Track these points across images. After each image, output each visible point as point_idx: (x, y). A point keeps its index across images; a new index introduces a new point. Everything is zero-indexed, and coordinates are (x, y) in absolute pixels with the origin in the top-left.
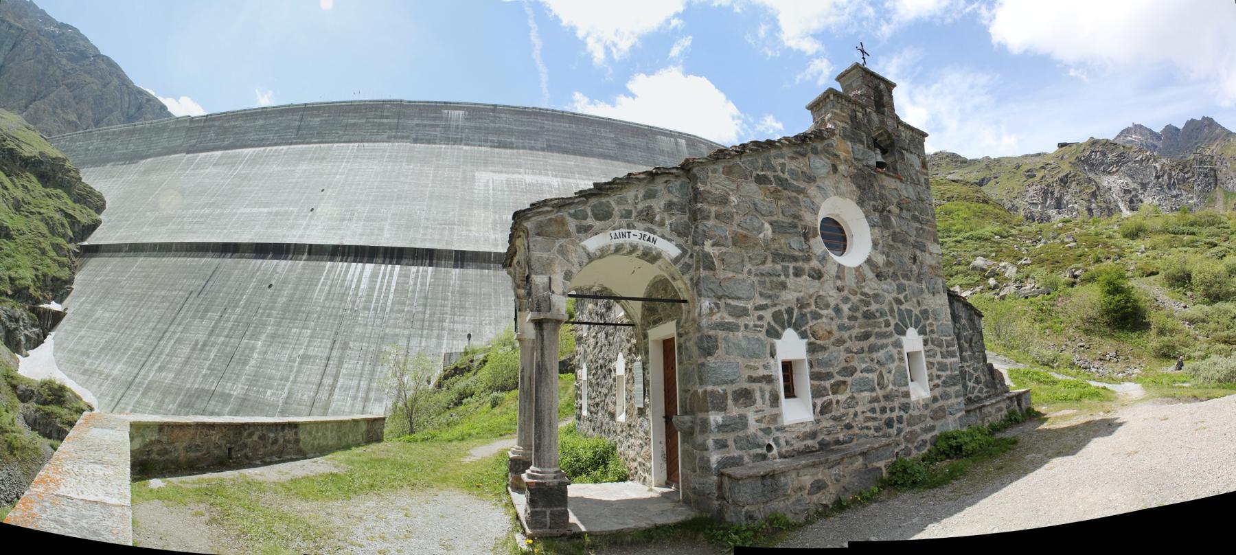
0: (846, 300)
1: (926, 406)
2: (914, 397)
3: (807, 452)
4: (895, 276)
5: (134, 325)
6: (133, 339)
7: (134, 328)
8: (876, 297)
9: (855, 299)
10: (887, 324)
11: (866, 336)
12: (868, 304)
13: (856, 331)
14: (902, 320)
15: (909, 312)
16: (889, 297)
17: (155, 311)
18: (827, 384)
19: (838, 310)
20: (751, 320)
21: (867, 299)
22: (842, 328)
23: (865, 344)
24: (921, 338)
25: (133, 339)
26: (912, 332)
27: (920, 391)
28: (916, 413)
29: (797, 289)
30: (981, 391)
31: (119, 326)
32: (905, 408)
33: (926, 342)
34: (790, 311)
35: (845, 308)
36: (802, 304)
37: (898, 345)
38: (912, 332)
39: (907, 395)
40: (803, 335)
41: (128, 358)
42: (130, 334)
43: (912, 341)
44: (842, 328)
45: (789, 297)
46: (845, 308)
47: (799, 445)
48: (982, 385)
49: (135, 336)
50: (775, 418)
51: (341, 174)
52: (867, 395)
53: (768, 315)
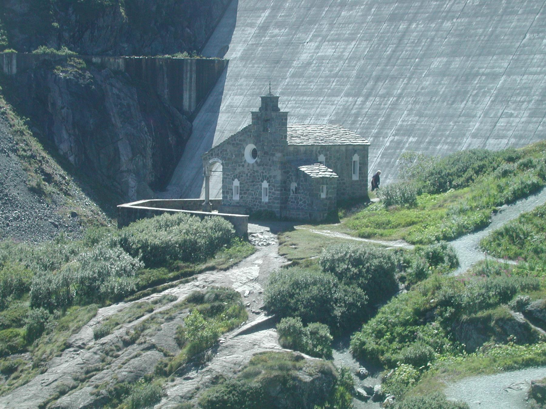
0: (249, 172)
1: (266, 203)
2: (263, 201)
3: (236, 206)
4: (263, 165)
5: (394, 71)
6: (394, 105)
7: (394, 78)
8: (257, 171)
9: (251, 172)
10: (259, 179)
11: (253, 182)
12: (254, 173)
13: (251, 180)
14: (263, 178)
15: (266, 176)
16: (260, 171)
17: (447, 25)
18: (243, 192)
19: (247, 175)
20: (229, 177)
21: (254, 172)
22: (247, 179)
23: (252, 184)
24: (268, 184)
25: (394, 105)
26: (265, 182)
27: (265, 199)
28: (262, 205)
29: (239, 170)
30: (305, 206)
31: (358, 77)
32: (260, 202)
33: (269, 185)
34: (237, 175)
35: (249, 174)
36: (240, 173)
37: (261, 185)
38: (265, 182)
39: (261, 199)
40: (239, 180)
41: (383, 155)
42: (388, 94)
43: (265, 184)
44: (247, 179)
45: (237, 172)
46: (249, 174)
47: (235, 204)
48: (306, 205)
49: (400, 96)
50: (232, 198)
51: (280, 25)
52: (251, 197)
53: (233, 176)
